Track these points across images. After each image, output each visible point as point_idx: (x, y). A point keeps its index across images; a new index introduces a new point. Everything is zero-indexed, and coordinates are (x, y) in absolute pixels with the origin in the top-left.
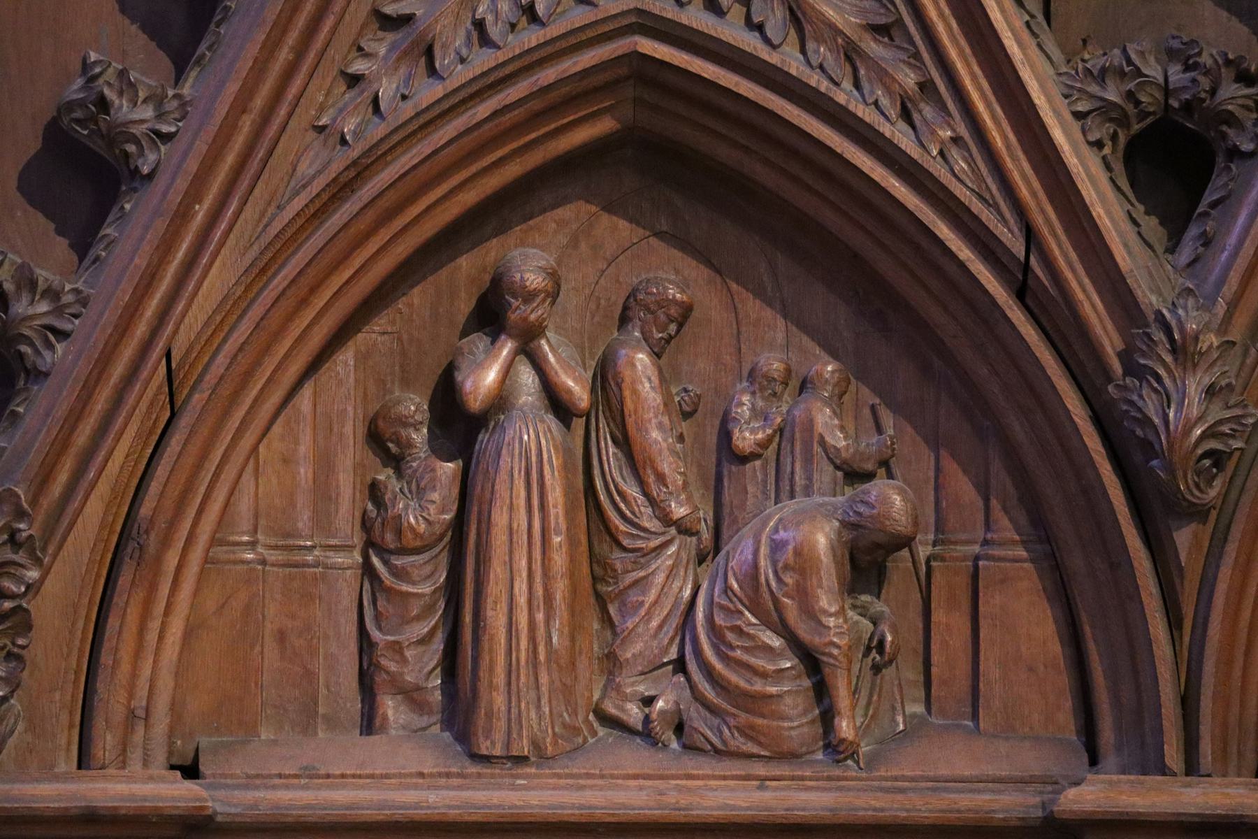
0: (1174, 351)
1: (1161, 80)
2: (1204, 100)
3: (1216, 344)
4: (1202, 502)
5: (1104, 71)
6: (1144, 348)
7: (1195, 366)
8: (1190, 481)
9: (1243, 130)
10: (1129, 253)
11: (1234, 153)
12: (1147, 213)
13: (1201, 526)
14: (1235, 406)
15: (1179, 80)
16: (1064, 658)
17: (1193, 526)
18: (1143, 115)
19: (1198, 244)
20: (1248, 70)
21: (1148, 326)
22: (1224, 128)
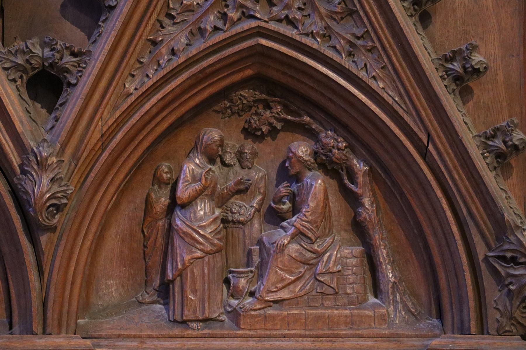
0: (38, 163)
1: (40, 55)
2: (57, 63)
3: (55, 162)
4: (51, 225)
5: (16, 51)
6: (27, 163)
7: (46, 170)
8: (44, 216)
9: (73, 75)
10: (23, 125)
11: (69, 85)
12: (42, 107)
13: (52, 234)
14: (63, 186)
15: (48, 55)
16: (3, 288)
17: (48, 234)
18: (33, 69)
19: (54, 121)
20: (74, 51)
21: (29, 154)
22: (65, 74)
